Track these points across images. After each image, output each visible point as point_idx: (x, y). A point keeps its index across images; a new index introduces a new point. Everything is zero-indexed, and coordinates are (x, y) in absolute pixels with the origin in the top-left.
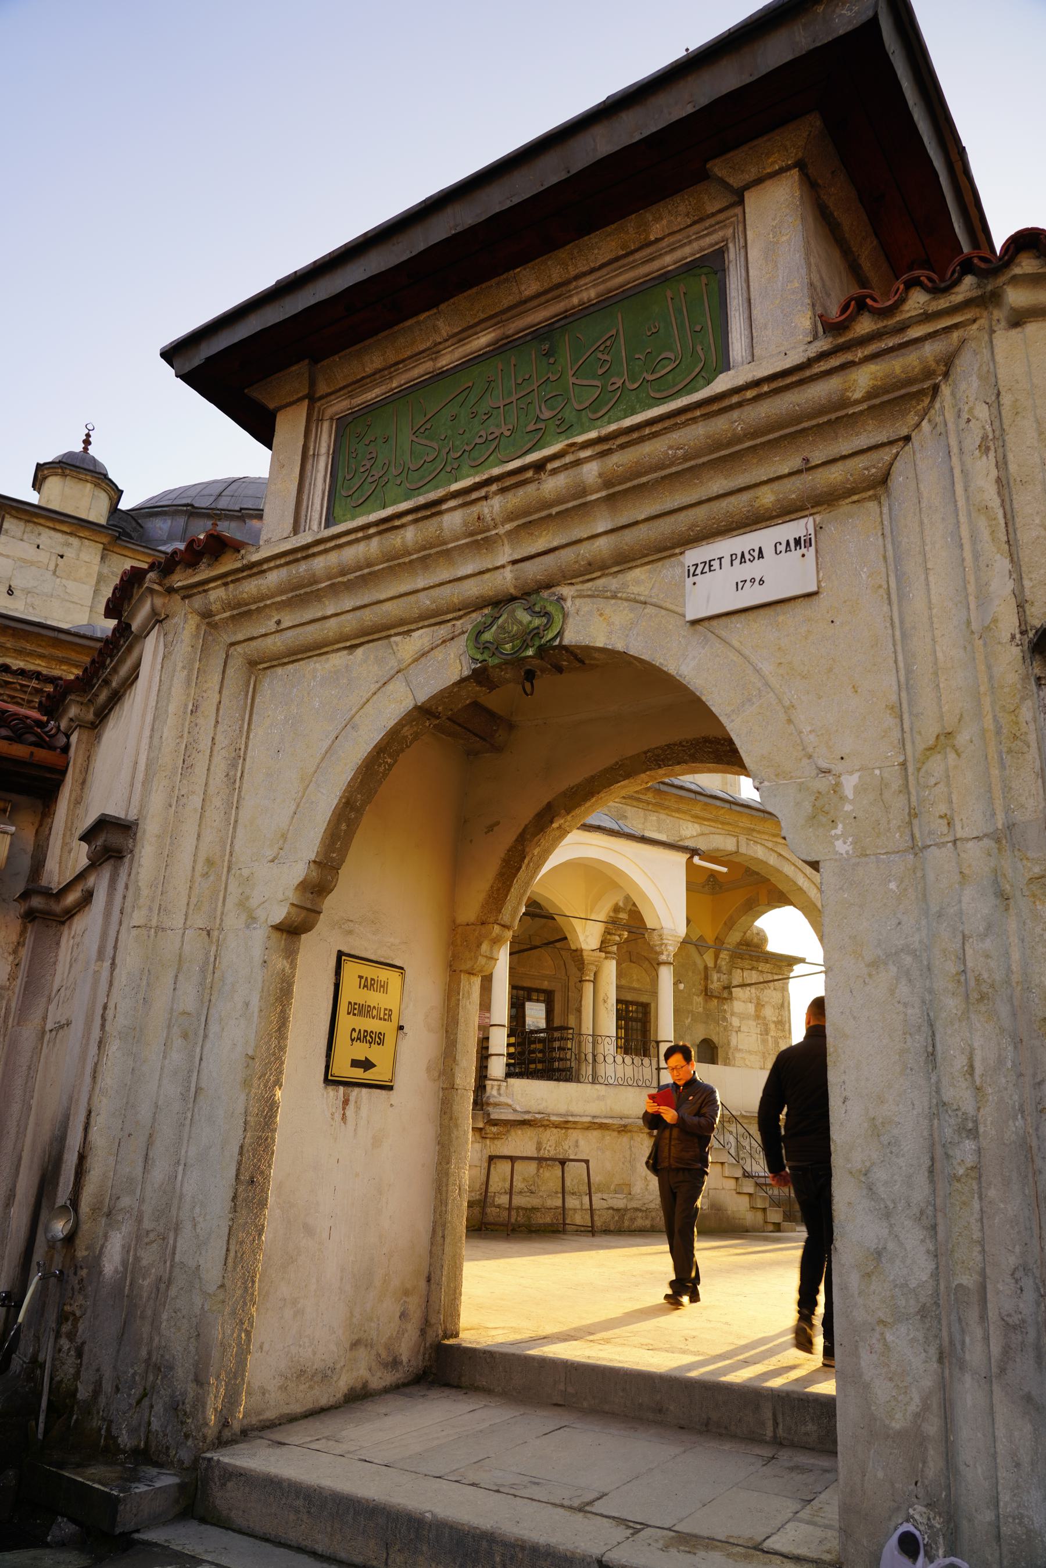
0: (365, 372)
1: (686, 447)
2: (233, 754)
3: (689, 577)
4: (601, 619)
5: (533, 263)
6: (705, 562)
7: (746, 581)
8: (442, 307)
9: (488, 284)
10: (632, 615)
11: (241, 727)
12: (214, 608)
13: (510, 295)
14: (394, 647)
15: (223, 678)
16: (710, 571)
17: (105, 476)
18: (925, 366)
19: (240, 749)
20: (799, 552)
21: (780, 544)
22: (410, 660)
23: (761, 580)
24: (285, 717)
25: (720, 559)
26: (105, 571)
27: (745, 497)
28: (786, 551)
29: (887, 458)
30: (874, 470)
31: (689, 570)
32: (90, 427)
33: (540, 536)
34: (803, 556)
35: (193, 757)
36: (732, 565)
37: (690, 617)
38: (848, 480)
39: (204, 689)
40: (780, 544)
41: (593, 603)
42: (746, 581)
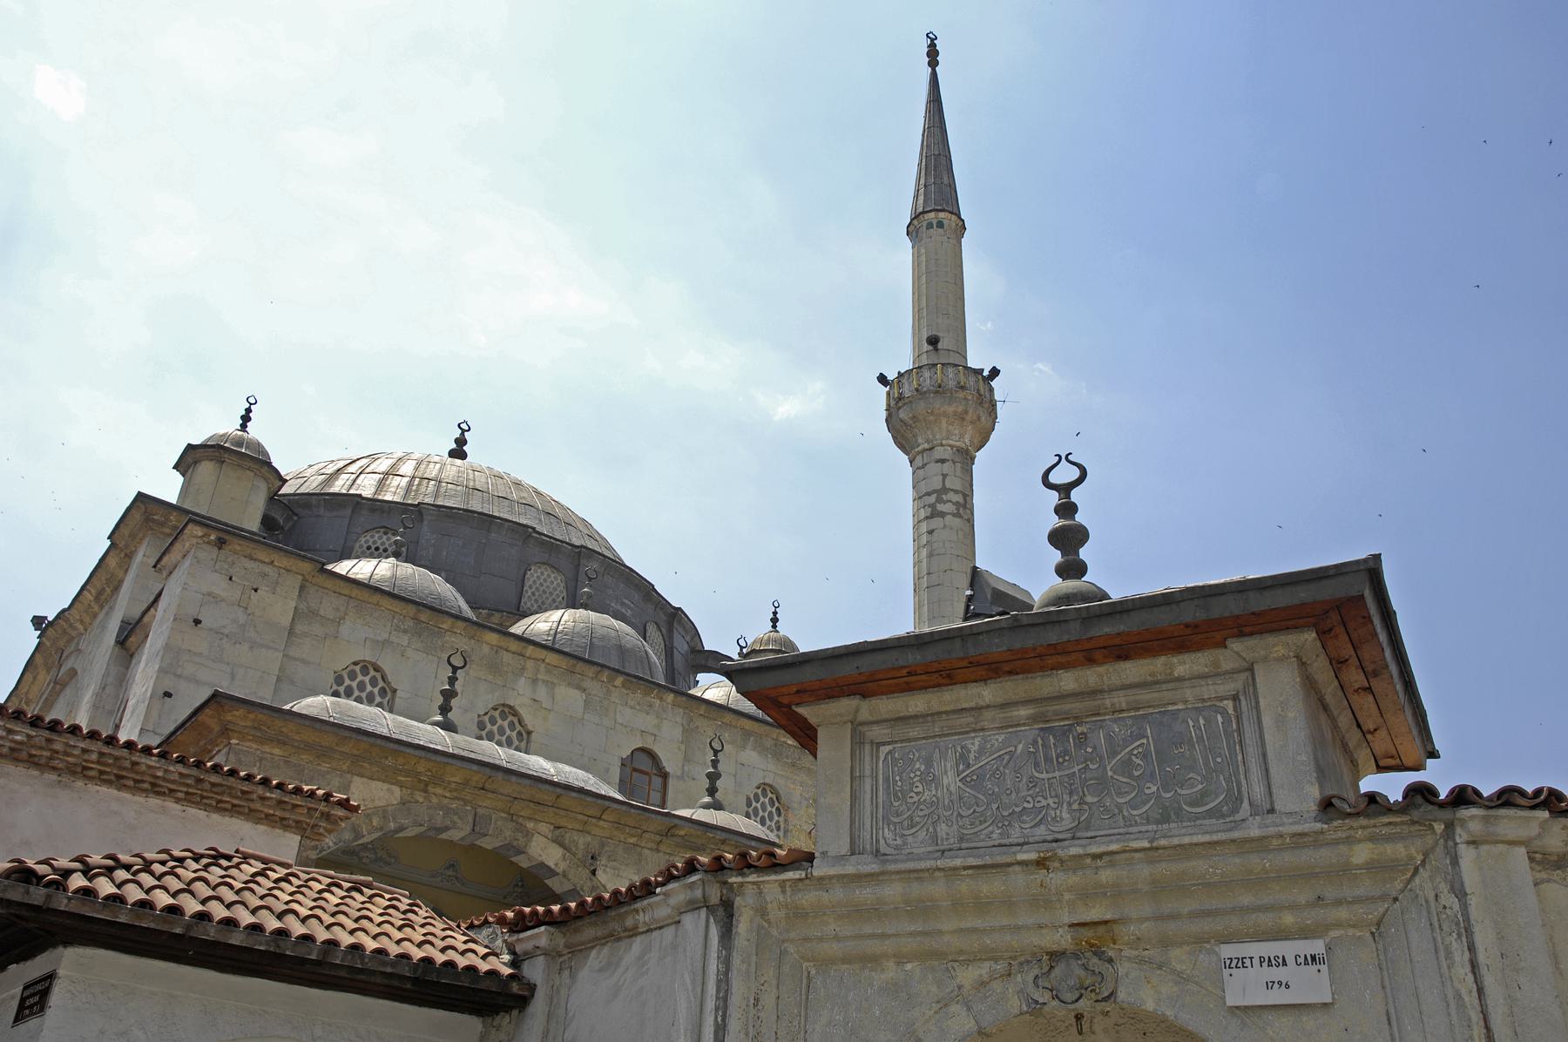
10: (1175, 989)
17: (269, 464)
20: (1315, 967)
23: (1286, 984)
24: (844, 1019)
25: (1251, 958)
26: (303, 606)
29: (1381, 910)
30: (1370, 916)
32: (252, 400)
36: (1261, 966)
37: (1230, 1002)
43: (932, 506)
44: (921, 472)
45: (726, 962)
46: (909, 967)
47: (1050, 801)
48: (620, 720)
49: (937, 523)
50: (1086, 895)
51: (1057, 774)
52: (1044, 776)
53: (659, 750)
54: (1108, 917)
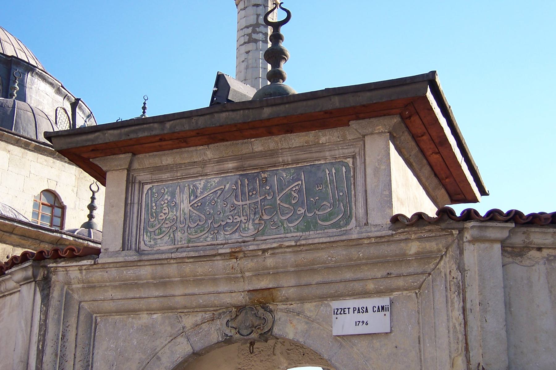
0: (162, 164)
1: (337, 258)
2: (86, 364)
3: (334, 314)
4: (292, 325)
5: (261, 139)
6: (342, 309)
7: (360, 322)
8: (210, 146)
9: (237, 142)
10: (306, 326)
11: (89, 349)
12: (81, 291)
13: (247, 149)
14: (180, 319)
15: (78, 321)
16: (344, 313)
18: (438, 248)
19: (89, 361)
20: (383, 313)
21: (375, 307)
22: (190, 328)
24: (116, 346)
25: (349, 309)
27: (361, 283)
28: (378, 311)
30: (415, 284)
31: (334, 311)
33: (263, 280)
34: (385, 315)
35: (63, 364)
36: (354, 313)
38: (405, 285)
39: (67, 326)
40: (375, 307)
41: (287, 316)
42: (360, 322)
43: (249, 35)
44: (243, 12)
45: (46, 314)
46: (155, 316)
47: (243, 218)
48: (32, 172)
49: (251, 46)
50: (259, 274)
51: (248, 202)
52: (240, 203)
53: (59, 192)
54: (270, 286)
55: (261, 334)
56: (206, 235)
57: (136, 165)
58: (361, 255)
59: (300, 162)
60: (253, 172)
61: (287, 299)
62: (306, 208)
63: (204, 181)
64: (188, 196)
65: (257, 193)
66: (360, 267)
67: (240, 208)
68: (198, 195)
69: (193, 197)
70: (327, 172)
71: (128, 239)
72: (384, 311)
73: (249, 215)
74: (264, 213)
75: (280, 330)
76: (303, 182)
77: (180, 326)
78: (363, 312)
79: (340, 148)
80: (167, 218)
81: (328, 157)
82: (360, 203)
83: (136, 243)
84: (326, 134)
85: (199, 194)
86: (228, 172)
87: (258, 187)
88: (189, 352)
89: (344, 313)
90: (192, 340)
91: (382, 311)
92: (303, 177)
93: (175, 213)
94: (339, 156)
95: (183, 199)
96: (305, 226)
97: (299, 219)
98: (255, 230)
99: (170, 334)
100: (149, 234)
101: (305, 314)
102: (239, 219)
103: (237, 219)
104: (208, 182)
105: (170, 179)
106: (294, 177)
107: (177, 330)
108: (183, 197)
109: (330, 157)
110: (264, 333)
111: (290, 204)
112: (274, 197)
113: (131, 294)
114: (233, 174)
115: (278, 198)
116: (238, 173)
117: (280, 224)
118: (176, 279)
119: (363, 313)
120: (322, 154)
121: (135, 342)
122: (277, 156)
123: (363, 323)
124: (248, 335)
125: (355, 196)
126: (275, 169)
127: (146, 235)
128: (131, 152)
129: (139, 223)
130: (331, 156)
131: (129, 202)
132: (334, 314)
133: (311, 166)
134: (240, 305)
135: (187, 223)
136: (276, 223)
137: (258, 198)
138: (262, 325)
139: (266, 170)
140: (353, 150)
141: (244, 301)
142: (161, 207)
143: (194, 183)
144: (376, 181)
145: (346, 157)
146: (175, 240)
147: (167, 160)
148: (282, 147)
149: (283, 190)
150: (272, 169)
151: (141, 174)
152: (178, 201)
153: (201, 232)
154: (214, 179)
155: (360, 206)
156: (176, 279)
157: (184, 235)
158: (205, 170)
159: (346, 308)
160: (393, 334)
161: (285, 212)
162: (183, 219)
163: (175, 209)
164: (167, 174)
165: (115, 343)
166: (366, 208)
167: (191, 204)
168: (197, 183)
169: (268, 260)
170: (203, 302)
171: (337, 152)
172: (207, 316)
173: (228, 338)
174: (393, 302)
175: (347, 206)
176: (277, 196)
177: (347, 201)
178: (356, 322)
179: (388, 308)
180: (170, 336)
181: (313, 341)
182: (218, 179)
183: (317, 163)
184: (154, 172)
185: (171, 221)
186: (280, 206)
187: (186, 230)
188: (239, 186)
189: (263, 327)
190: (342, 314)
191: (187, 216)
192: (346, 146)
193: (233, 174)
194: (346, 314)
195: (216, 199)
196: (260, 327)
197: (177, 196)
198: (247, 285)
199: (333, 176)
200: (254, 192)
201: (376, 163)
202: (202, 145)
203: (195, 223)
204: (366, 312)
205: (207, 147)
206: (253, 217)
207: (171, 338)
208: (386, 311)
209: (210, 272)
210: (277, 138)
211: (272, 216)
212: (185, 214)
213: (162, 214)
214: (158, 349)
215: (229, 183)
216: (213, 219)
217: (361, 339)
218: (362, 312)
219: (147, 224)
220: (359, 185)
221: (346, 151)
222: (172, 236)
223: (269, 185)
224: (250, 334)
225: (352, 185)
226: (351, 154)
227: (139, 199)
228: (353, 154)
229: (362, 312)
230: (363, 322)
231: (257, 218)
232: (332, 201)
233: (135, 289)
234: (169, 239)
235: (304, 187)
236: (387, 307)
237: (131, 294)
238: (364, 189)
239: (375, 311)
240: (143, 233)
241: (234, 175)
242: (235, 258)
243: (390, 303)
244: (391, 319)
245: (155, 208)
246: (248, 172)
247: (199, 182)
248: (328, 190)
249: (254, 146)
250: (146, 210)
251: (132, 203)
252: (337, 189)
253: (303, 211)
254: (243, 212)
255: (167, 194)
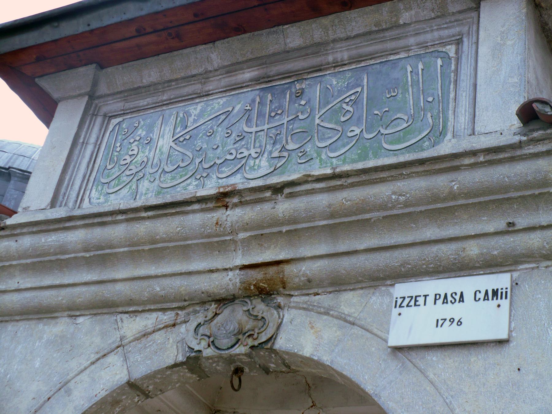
1: (408, 195)
3: (396, 307)
4: (312, 331)
6: (412, 297)
7: (445, 320)
8: (218, 43)
10: (338, 333)
14: (119, 323)
16: (415, 305)
20: (495, 302)
21: (480, 292)
22: (132, 338)
25: (425, 296)
31: (396, 301)
34: (499, 306)
36: (435, 303)
38: (544, 247)
40: (480, 292)
42: (445, 320)
55: (252, 347)
56: (189, 181)
57: (103, 89)
58: (455, 188)
59: (364, 60)
60: (283, 82)
61: (309, 281)
62: (364, 127)
63: (202, 104)
64: (172, 128)
65: (283, 113)
66: (454, 214)
67: (251, 138)
68: (189, 125)
69: (181, 127)
70: (409, 69)
71: (65, 194)
72: (497, 299)
73: (264, 146)
74: (289, 141)
75: (289, 340)
76: (365, 87)
77: (118, 335)
78: (453, 301)
79: (435, 28)
80: (134, 161)
81: (412, 48)
82: (464, 107)
83: (76, 201)
84: (410, 6)
85: (191, 123)
86: (242, 87)
87: (287, 104)
88: (121, 380)
89: (415, 305)
90: (132, 359)
91: (493, 299)
92: (365, 80)
93: (147, 154)
94: (432, 44)
95: (164, 133)
96: (358, 154)
97: (348, 143)
98: (271, 167)
99: (96, 349)
100: (100, 188)
101: (340, 311)
102: (246, 153)
103: (243, 153)
104: (208, 106)
105: (151, 106)
106: (350, 83)
107: (110, 342)
108: (164, 130)
109: (415, 47)
110: (259, 344)
111: (337, 122)
112: (311, 115)
113: (48, 281)
114: (250, 89)
115: (317, 117)
116: (258, 87)
117: (316, 154)
118: (122, 250)
119: (453, 303)
120: (401, 43)
121: (38, 364)
122: (325, 53)
123: (453, 322)
124: (228, 349)
125: (455, 100)
126: (321, 74)
127: (95, 190)
128: (95, 63)
129: (89, 172)
130: (418, 45)
131: (81, 141)
132: (396, 307)
133: (382, 64)
134: (224, 296)
135: (162, 166)
136: (307, 154)
137: (284, 119)
138: (257, 331)
139: (306, 77)
140: (458, 29)
141: (231, 287)
142: (128, 148)
143: (187, 109)
144: (495, 63)
145: (444, 44)
146: (137, 192)
147: (150, 76)
148: (336, 36)
149: (328, 103)
150: (315, 75)
151: (109, 103)
152: (156, 135)
153: (181, 178)
154: (219, 100)
155: (463, 112)
156: (122, 250)
157: (153, 184)
158: (206, 87)
159: (420, 296)
160: (515, 343)
161: (326, 136)
162: (157, 161)
163: (148, 147)
164: (148, 99)
165: (6, 366)
166: (472, 113)
167: (175, 138)
168: (191, 108)
169: (281, 207)
170: (161, 290)
171: (429, 37)
172: (165, 318)
173: (194, 354)
174: (517, 284)
175: (439, 117)
176: (317, 113)
177: (441, 108)
178: (438, 320)
179: (506, 292)
180: (97, 353)
181: (349, 360)
182: (224, 100)
183: (392, 58)
184: (128, 98)
185: (137, 166)
186: (320, 128)
187: (157, 177)
188: (257, 106)
189: (258, 333)
190: (411, 306)
191: (165, 156)
192: (446, 23)
193: (250, 89)
194: (419, 305)
195: (215, 127)
196: (252, 333)
197: (156, 129)
198: (240, 257)
199: (418, 74)
200: (279, 112)
201: (497, 37)
202: (205, 44)
203: (174, 165)
204: (459, 302)
205: (212, 46)
206: (271, 149)
207: (97, 356)
208: (501, 298)
209: (178, 233)
210: (325, 21)
211: (303, 144)
212: (162, 153)
213: (127, 157)
214: (71, 375)
215: (242, 102)
216: (204, 156)
217: (446, 354)
218: (451, 301)
219: (100, 174)
220: (463, 80)
221: (446, 33)
222: (134, 187)
223: (307, 98)
224: (232, 347)
225: (452, 84)
226: (453, 39)
227: (98, 138)
228: (458, 37)
229: (451, 301)
230: (452, 320)
231: (276, 150)
232: (412, 111)
233: (56, 271)
234: (129, 192)
235: (365, 95)
236: (504, 291)
237: (48, 281)
238: (472, 83)
239: (479, 299)
240: (92, 187)
241: (251, 91)
242: (224, 206)
243: (512, 286)
244: (510, 316)
245: (118, 149)
246: (274, 84)
247: (195, 107)
248: (407, 96)
249: (287, 37)
250: (105, 154)
251: (85, 143)
252: (423, 93)
253: (358, 131)
254: (255, 141)
255: (141, 128)
